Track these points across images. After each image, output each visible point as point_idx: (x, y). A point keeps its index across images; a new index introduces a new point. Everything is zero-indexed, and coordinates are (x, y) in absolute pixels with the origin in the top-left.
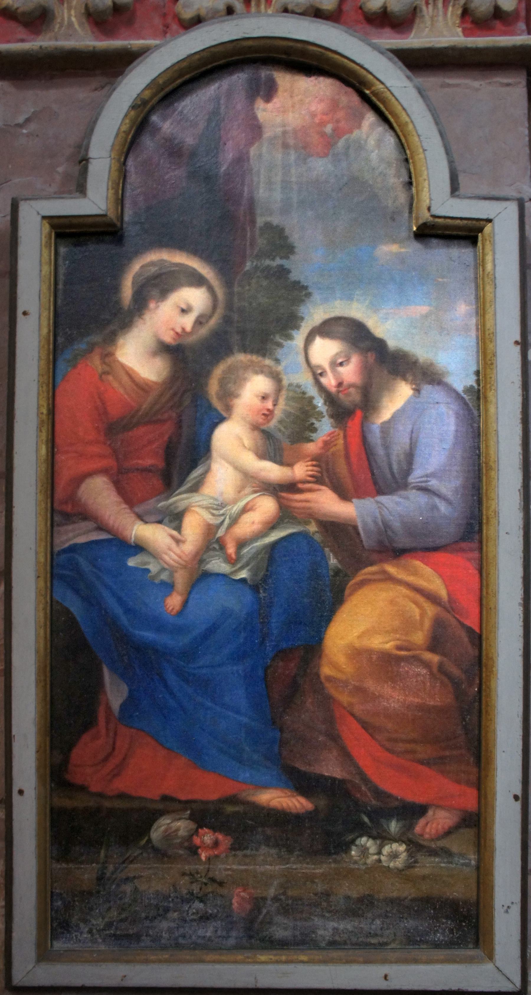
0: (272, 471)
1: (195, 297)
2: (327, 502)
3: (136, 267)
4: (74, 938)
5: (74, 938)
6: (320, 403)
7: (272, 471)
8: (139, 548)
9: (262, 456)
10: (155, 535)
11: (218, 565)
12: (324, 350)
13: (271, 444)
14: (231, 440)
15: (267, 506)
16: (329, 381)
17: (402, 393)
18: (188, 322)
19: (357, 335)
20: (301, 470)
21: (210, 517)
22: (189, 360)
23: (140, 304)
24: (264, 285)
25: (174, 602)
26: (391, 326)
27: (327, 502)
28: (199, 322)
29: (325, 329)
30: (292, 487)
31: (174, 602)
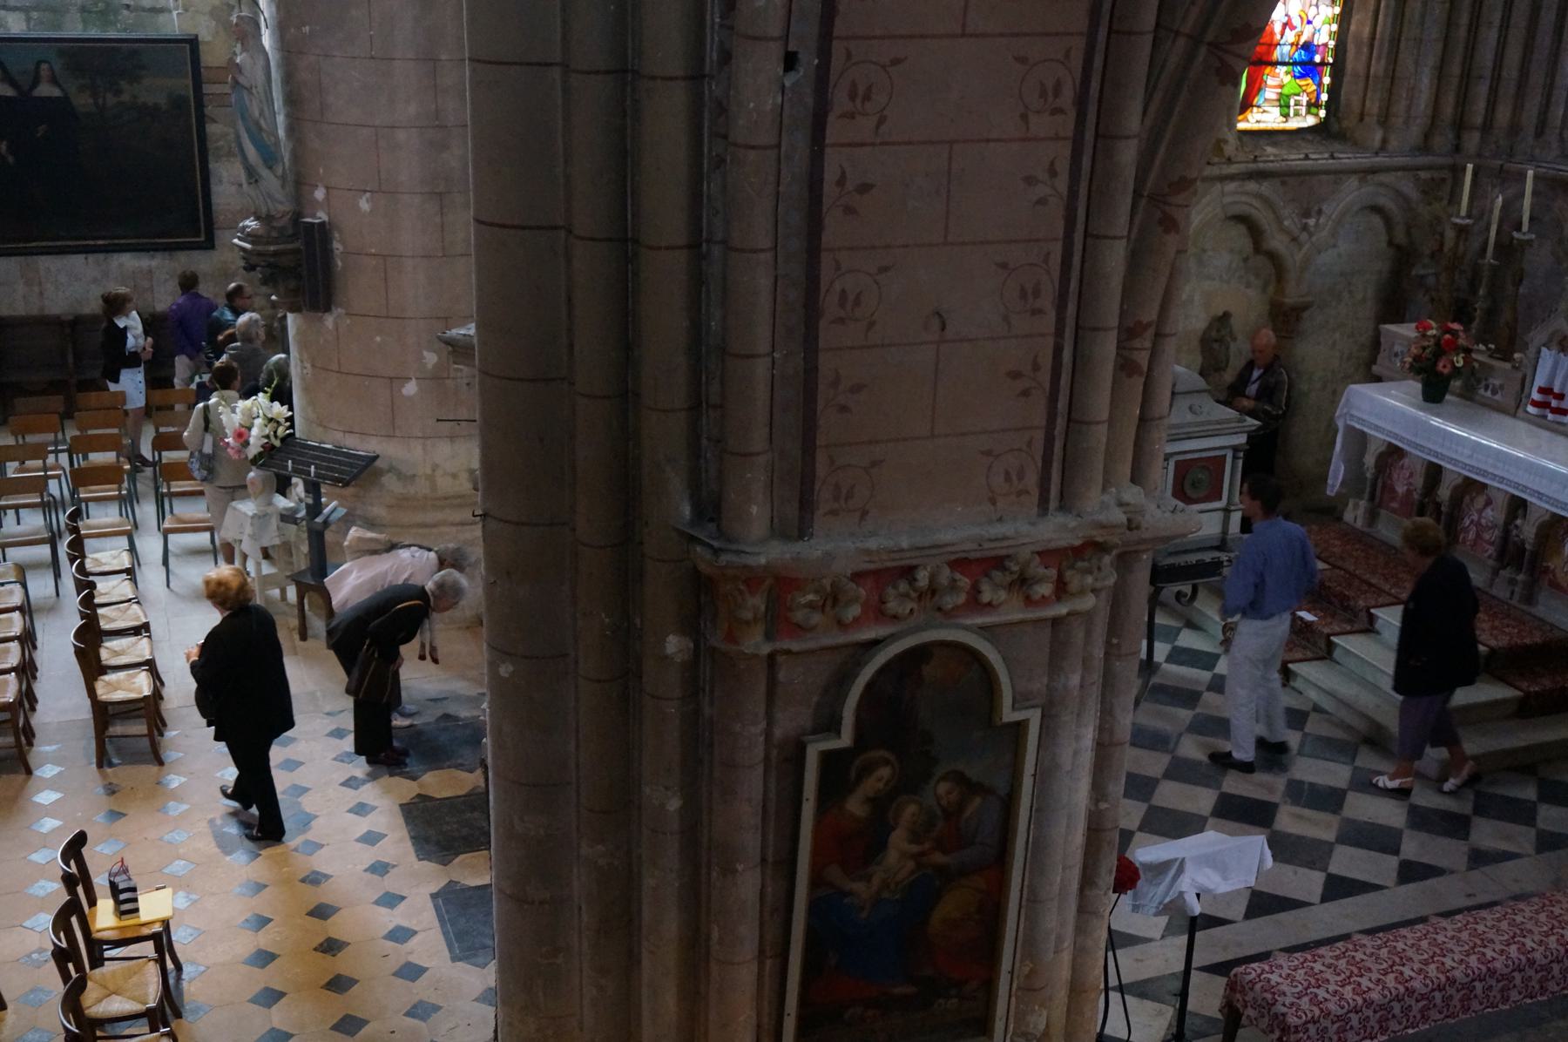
0: (915, 848)
1: (885, 772)
2: (939, 858)
3: (857, 762)
4: (1252, 389)
5: (1252, 389)
6: (939, 812)
7: (915, 848)
8: (850, 893)
9: (911, 842)
10: (858, 886)
11: (886, 895)
12: (943, 788)
13: (915, 837)
14: (898, 840)
15: (911, 864)
16: (944, 802)
17: (978, 801)
18: (881, 785)
19: (960, 778)
20: (927, 846)
21: (100, 902)
22: (881, 806)
23: (860, 778)
24: (889, 605)
25: (864, 915)
26: (974, 772)
27: (939, 858)
28: (886, 784)
29: (944, 778)
30: (922, 854)
31: (864, 915)
